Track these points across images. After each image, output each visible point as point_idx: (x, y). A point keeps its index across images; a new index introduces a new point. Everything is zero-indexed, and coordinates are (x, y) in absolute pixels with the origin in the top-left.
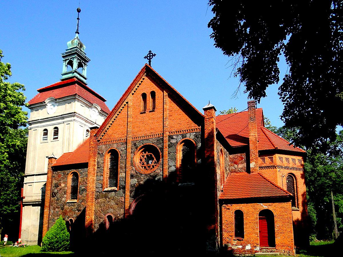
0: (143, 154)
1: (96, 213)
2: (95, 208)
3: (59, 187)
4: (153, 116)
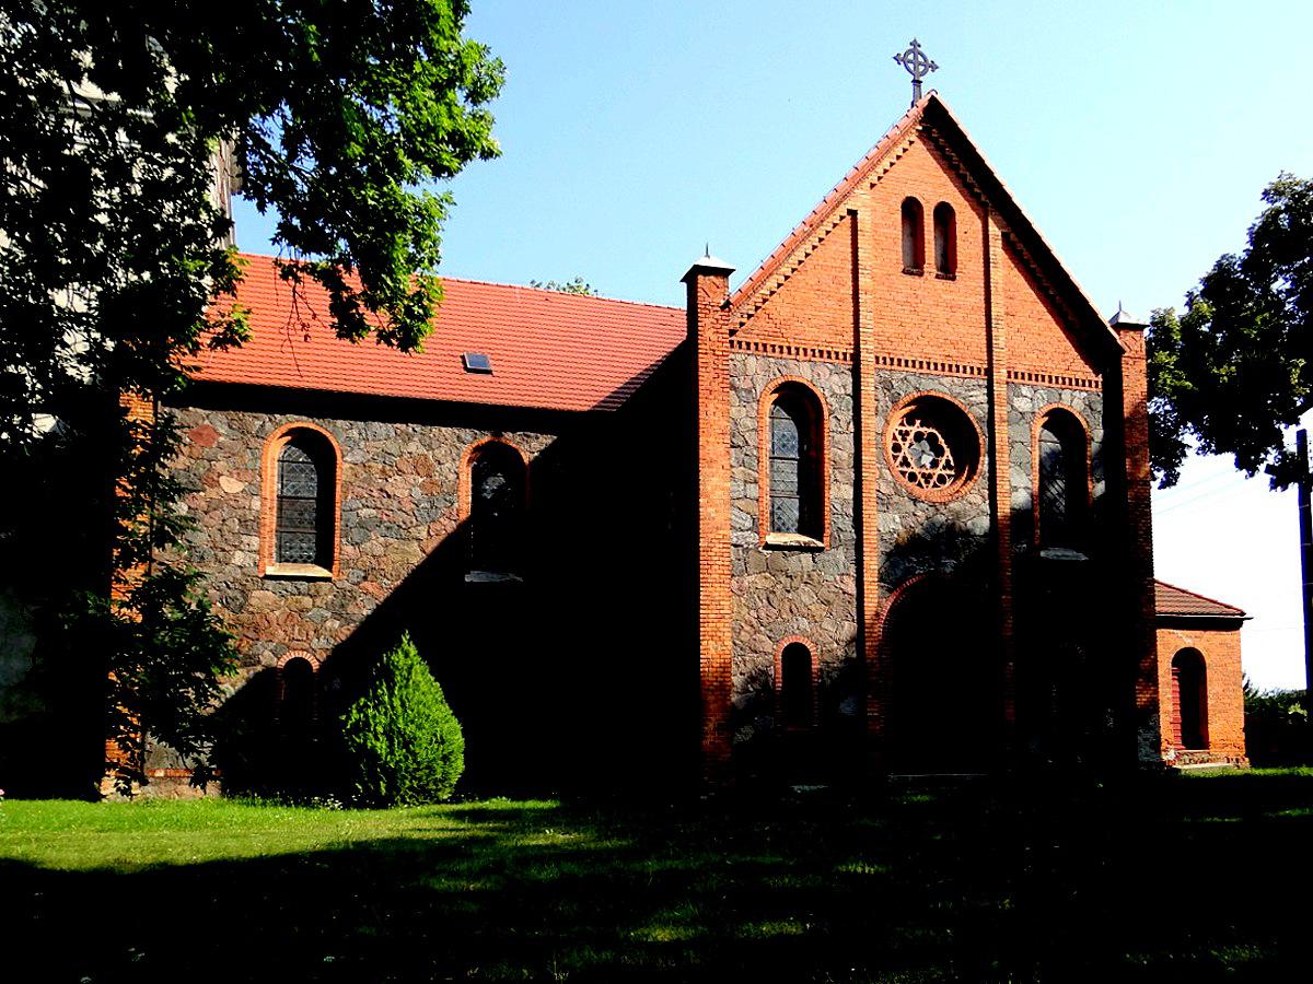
3: (204, 491)
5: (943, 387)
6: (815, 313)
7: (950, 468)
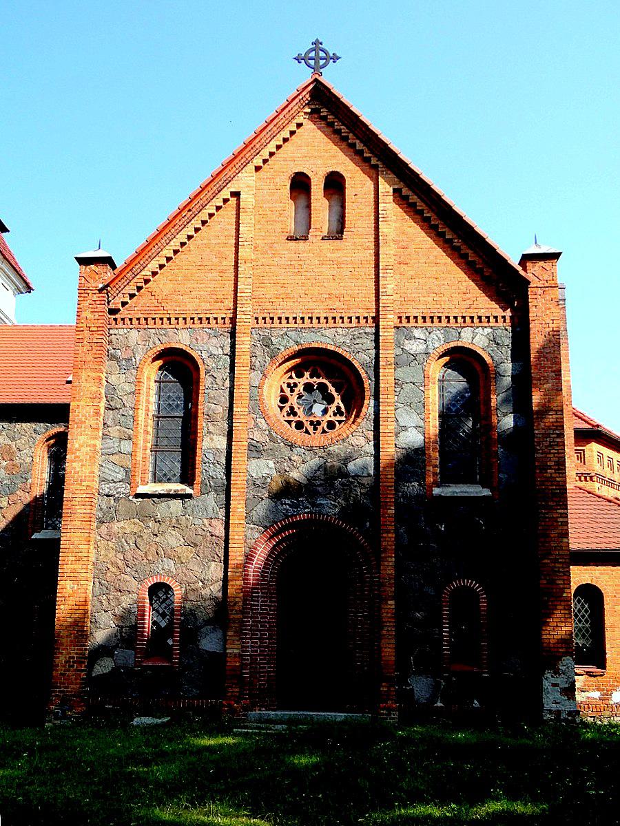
0: (291, 377)
1: (100, 574)
2: (98, 553)
4: (339, 254)
5: (326, 339)
6: (195, 286)
7: (341, 414)
